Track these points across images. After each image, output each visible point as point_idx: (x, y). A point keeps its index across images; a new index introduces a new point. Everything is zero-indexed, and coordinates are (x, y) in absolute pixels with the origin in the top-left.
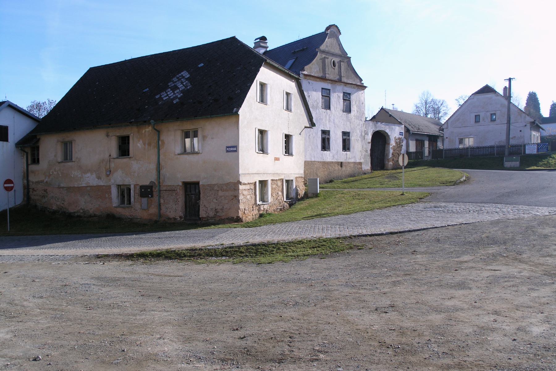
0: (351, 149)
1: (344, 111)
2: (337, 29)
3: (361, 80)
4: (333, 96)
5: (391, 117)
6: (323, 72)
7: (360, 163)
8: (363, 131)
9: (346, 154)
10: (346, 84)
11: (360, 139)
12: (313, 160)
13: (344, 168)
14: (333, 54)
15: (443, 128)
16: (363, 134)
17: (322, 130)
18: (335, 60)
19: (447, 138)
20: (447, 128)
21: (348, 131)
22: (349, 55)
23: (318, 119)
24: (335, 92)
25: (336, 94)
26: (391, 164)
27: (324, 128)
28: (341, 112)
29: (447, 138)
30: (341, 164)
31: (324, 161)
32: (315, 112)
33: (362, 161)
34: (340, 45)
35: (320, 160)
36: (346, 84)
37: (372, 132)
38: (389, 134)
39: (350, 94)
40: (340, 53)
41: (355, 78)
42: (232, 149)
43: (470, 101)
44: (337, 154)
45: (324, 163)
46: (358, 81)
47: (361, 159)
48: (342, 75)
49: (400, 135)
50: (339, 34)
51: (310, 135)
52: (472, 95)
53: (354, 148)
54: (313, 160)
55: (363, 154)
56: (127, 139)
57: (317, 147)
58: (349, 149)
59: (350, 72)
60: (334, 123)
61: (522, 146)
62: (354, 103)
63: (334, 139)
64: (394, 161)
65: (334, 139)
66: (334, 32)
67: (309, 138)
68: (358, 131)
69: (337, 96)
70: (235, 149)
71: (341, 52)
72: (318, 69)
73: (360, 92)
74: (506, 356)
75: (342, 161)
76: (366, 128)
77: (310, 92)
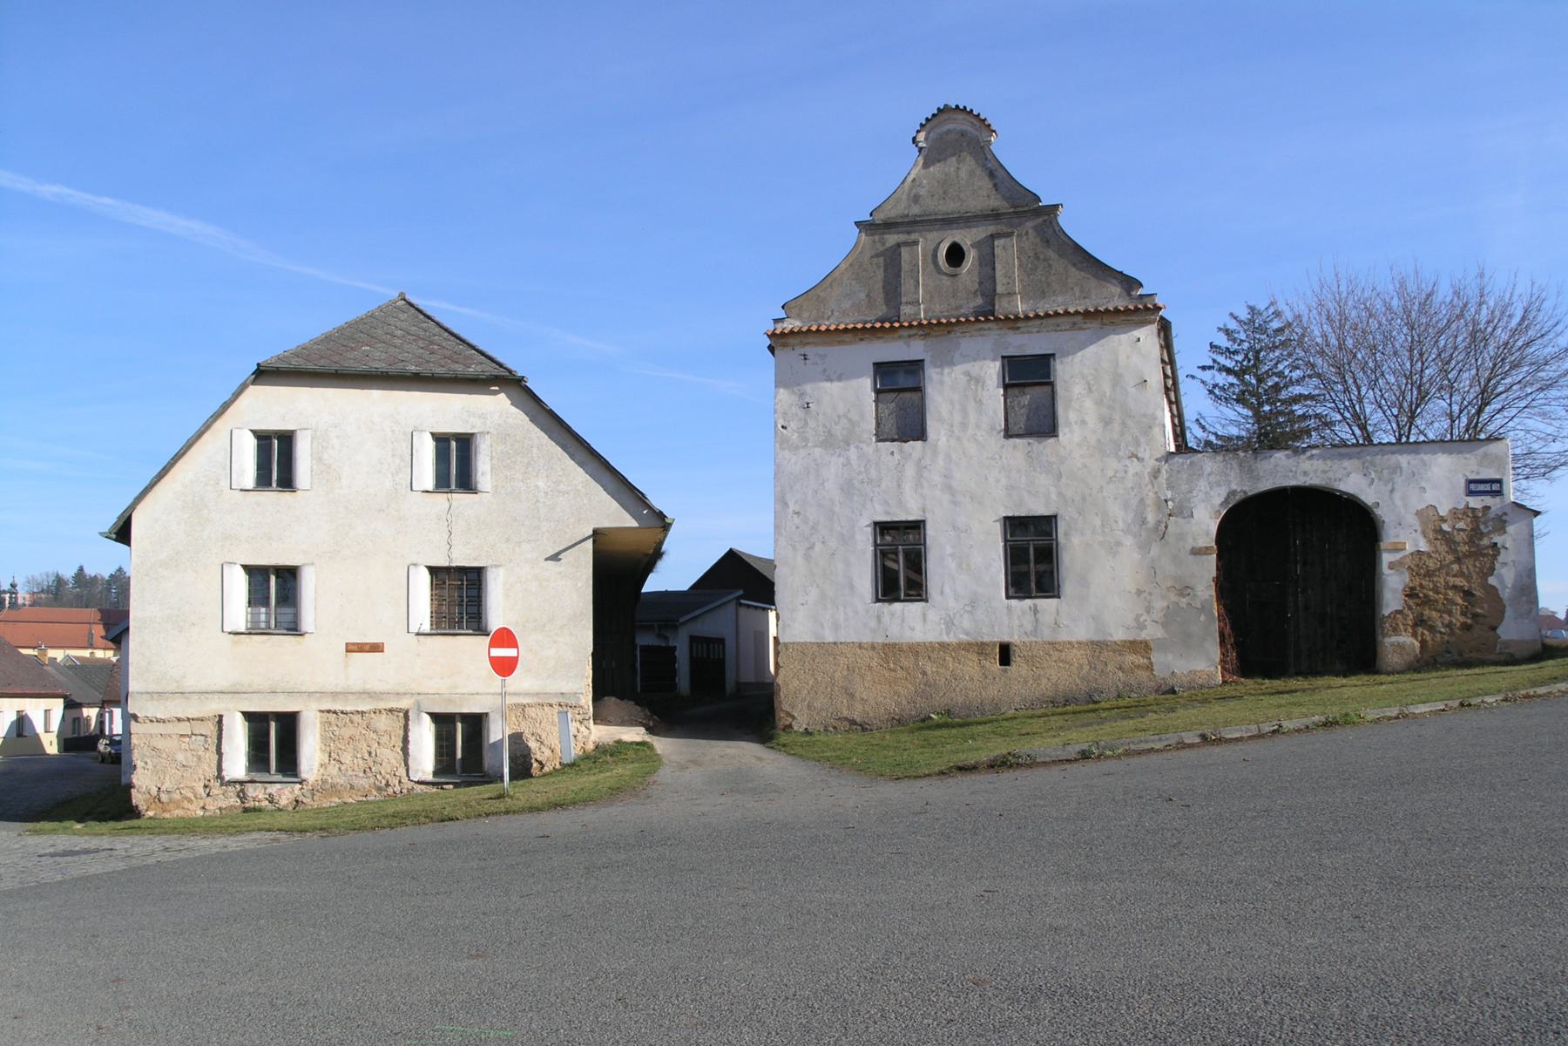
0: (1068, 585)
6: (887, 301)
7: (1140, 647)
9: (1035, 611)
11: (1129, 541)
12: (832, 640)
13: (1018, 667)
17: (876, 524)
18: (958, 239)
21: (1039, 509)
22: (1046, 201)
23: (856, 484)
24: (952, 364)
25: (959, 370)
26: (1401, 647)
27: (888, 513)
28: (997, 441)
31: (887, 641)
32: (842, 460)
33: (1152, 632)
35: (867, 638)
37: (1218, 500)
40: (995, 202)
41: (1093, 283)
42: (1482, 487)
44: (970, 612)
45: (891, 651)
47: (1141, 627)
50: (985, 133)
51: (812, 547)
54: (829, 638)
55: (1159, 604)
56: (1054, 520)
57: (852, 587)
59: (1058, 264)
60: (949, 488)
63: (949, 550)
65: (949, 550)
67: (807, 557)
69: (964, 379)
70: (1495, 487)
71: (1005, 198)
72: (863, 296)
73: (1124, 337)
74: (1531, 318)
75: (1006, 639)
77: (808, 388)
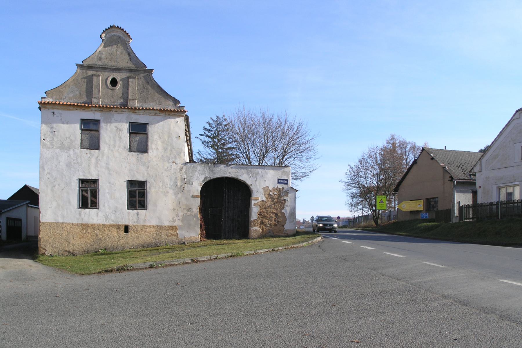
1: (135, 148)
2: (119, 30)
3: (176, 102)
4: (107, 129)
5: (434, 160)
7: (174, 228)
8: (179, 178)
9: (138, 214)
10: (134, 110)
11: (171, 192)
13: (131, 234)
14: (110, 68)
15: (475, 171)
16: (179, 184)
19: (480, 187)
20: (480, 172)
22: (148, 67)
24: (111, 122)
26: (256, 230)
29: (480, 187)
30: (127, 229)
33: (178, 223)
34: (131, 55)
35: (75, 222)
36: (134, 110)
38: (249, 182)
39: (97, 122)
40: (130, 65)
41: (163, 100)
43: (515, 122)
45: (84, 226)
46: (171, 103)
48: (130, 97)
49: (279, 183)
50: (128, 38)
52: (517, 112)
53: (155, 205)
54: (60, 220)
55: (181, 214)
58: (143, 206)
60: (107, 168)
61: (498, 204)
62: (156, 137)
64: (265, 225)
65: (107, 191)
66: (119, 37)
67: (52, 190)
68: (167, 180)
69: (115, 129)
72: (77, 93)
75: (127, 224)
76: (186, 174)
